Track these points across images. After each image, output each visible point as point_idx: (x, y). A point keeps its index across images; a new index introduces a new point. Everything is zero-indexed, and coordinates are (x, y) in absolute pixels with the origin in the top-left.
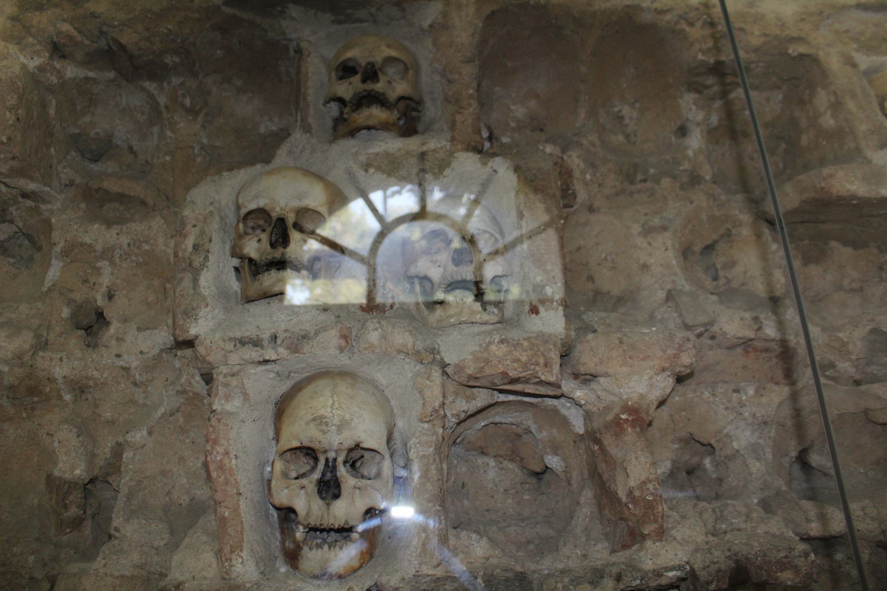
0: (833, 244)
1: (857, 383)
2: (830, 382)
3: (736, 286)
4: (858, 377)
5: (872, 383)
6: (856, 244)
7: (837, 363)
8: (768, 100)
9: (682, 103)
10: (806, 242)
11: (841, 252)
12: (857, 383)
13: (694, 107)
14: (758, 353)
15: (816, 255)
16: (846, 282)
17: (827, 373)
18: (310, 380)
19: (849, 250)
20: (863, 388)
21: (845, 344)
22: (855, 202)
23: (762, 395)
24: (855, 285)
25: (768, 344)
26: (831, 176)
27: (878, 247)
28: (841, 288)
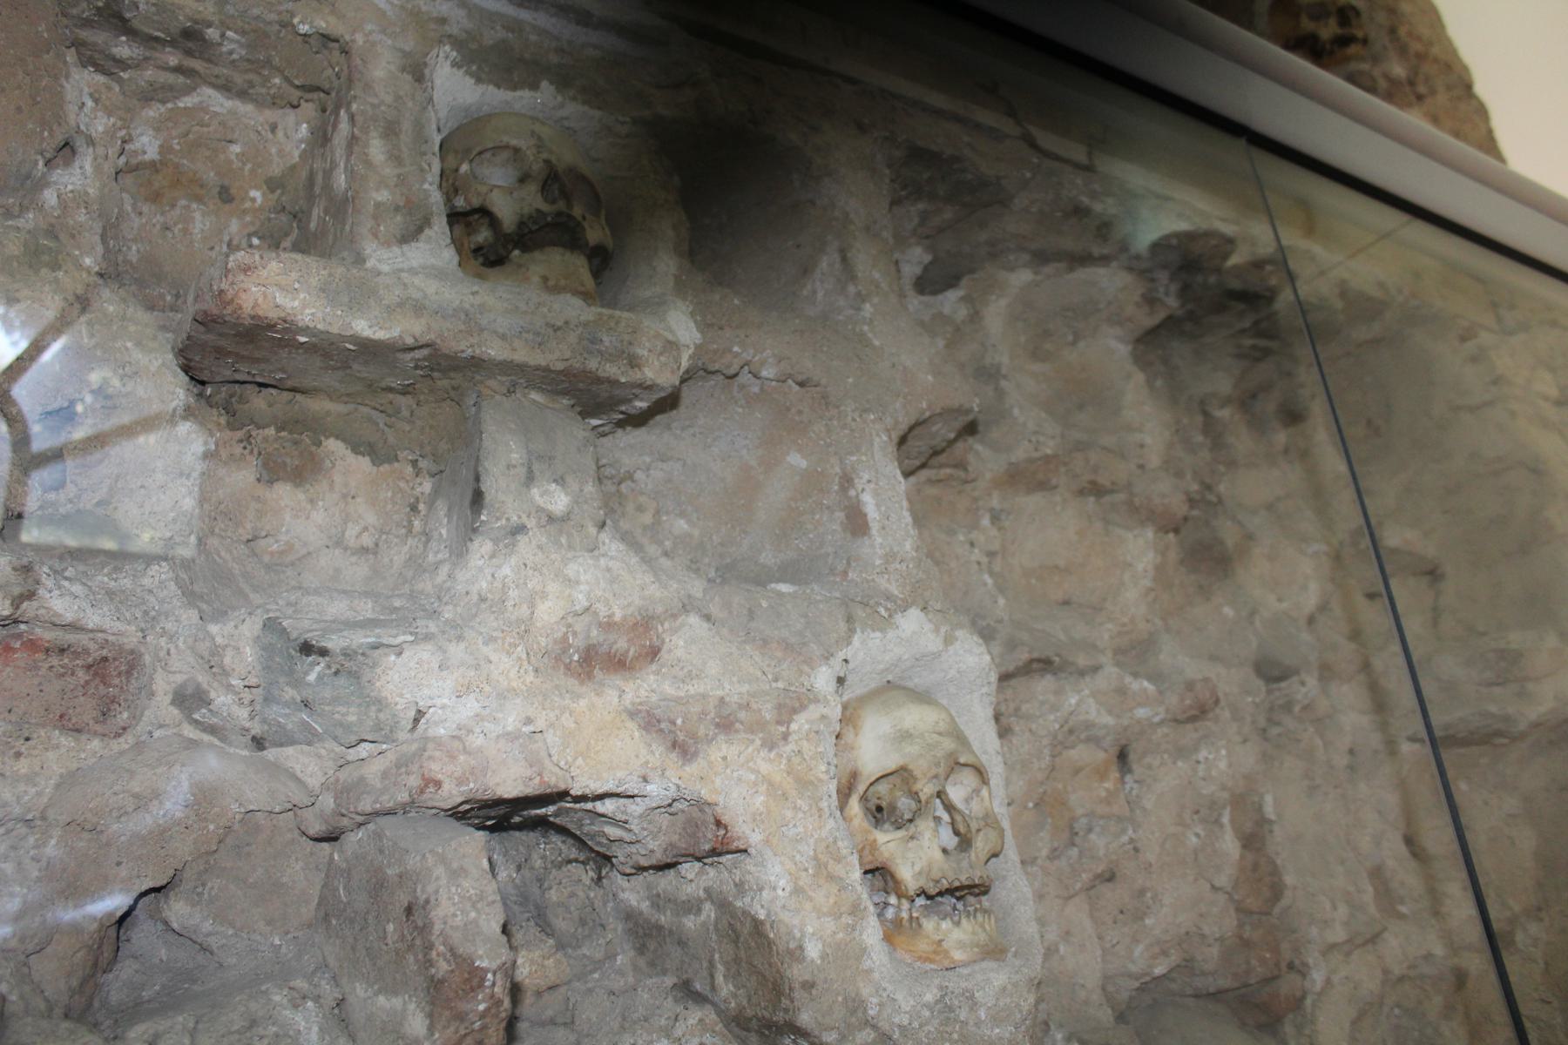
0: (333, 445)
1: (259, 743)
2: (206, 738)
3: (89, 507)
4: (257, 729)
5: (281, 745)
6: (377, 453)
7: (213, 695)
8: (274, 128)
9: (70, 92)
10: (271, 431)
11: (348, 466)
12: (259, 743)
13: (90, 103)
14: (40, 656)
15: (294, 466)
16: (352, 531)
17: (196, 716)
18: (563, 831)
19: (364, 463)
20: (271, 754)
21: (217, 651)
22: (303, 339)
23: (18, 755)
24: (367, 540)
25: (71, 638)
26: (247, 269)
27: (414, 463)
28: (339, 542)
